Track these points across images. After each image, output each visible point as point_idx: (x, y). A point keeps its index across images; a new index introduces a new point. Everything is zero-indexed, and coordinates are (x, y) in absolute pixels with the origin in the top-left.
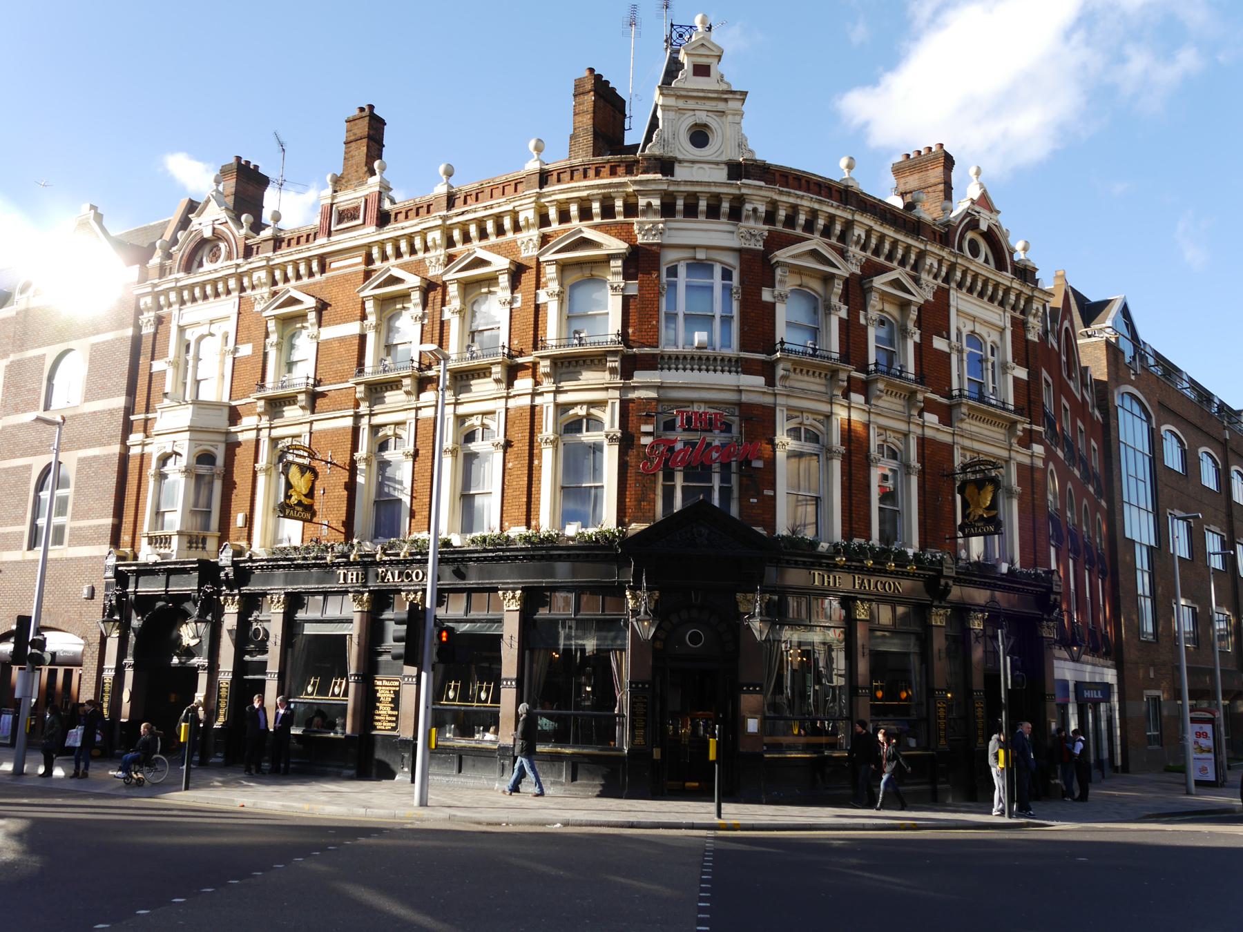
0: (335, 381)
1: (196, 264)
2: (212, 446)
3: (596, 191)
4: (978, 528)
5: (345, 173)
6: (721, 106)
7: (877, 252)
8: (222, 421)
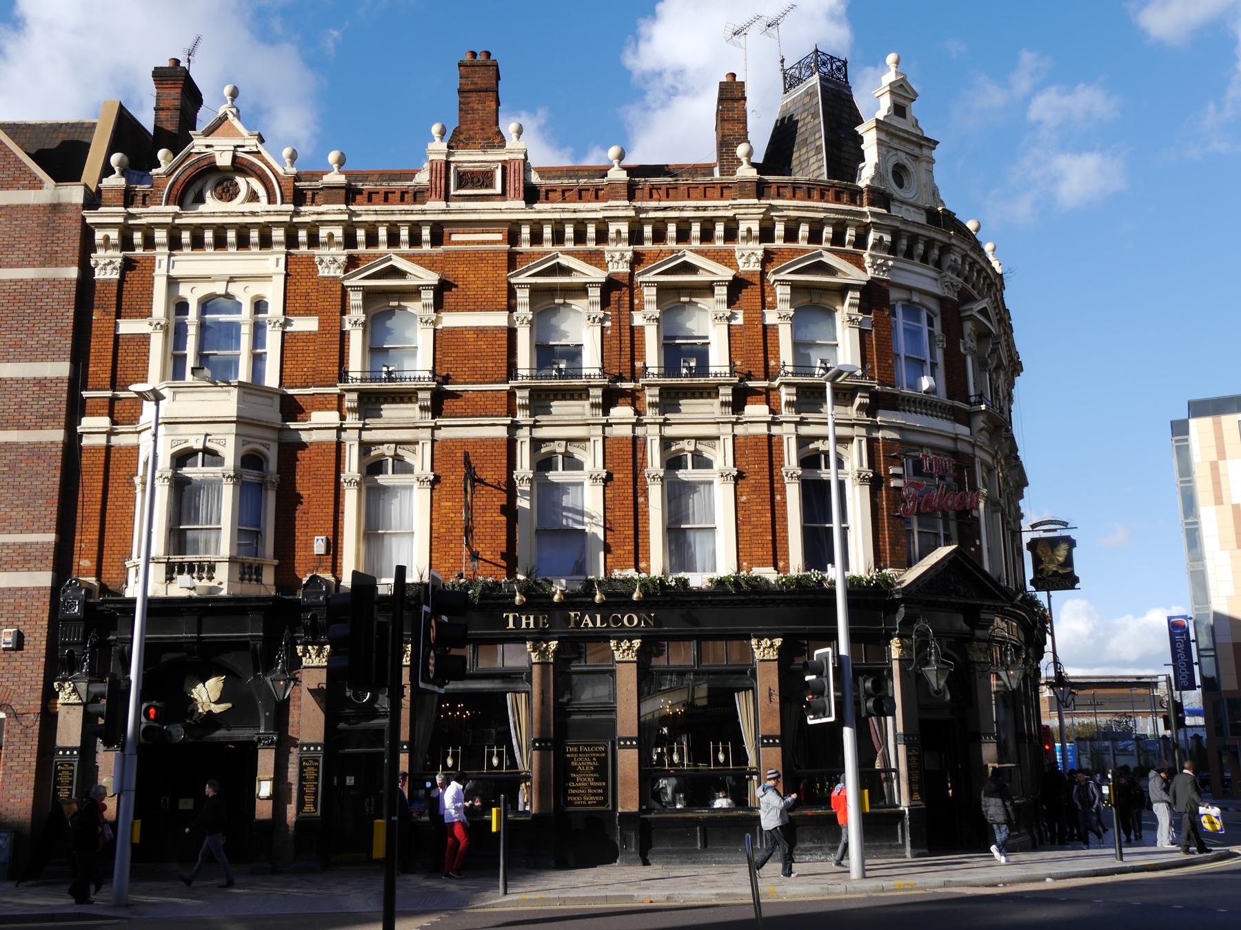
1: (191, 196)
2: (263, 445)
3: (832, 216)
5: (464, 127)
8: (273, 414)
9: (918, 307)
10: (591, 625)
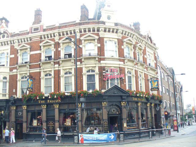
7: (125, 34)
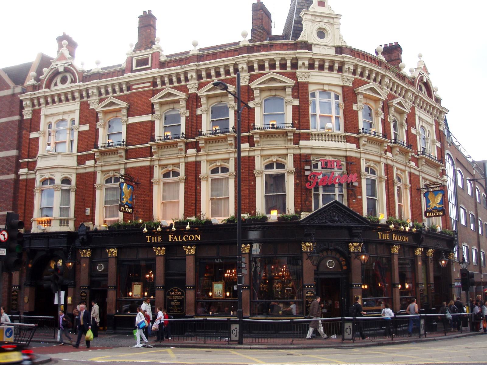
0: (138, 143)
2: (69, 175)
4: (434, 213)
6: (331, 21)
9: (329, 91)
10: (177, 240)
